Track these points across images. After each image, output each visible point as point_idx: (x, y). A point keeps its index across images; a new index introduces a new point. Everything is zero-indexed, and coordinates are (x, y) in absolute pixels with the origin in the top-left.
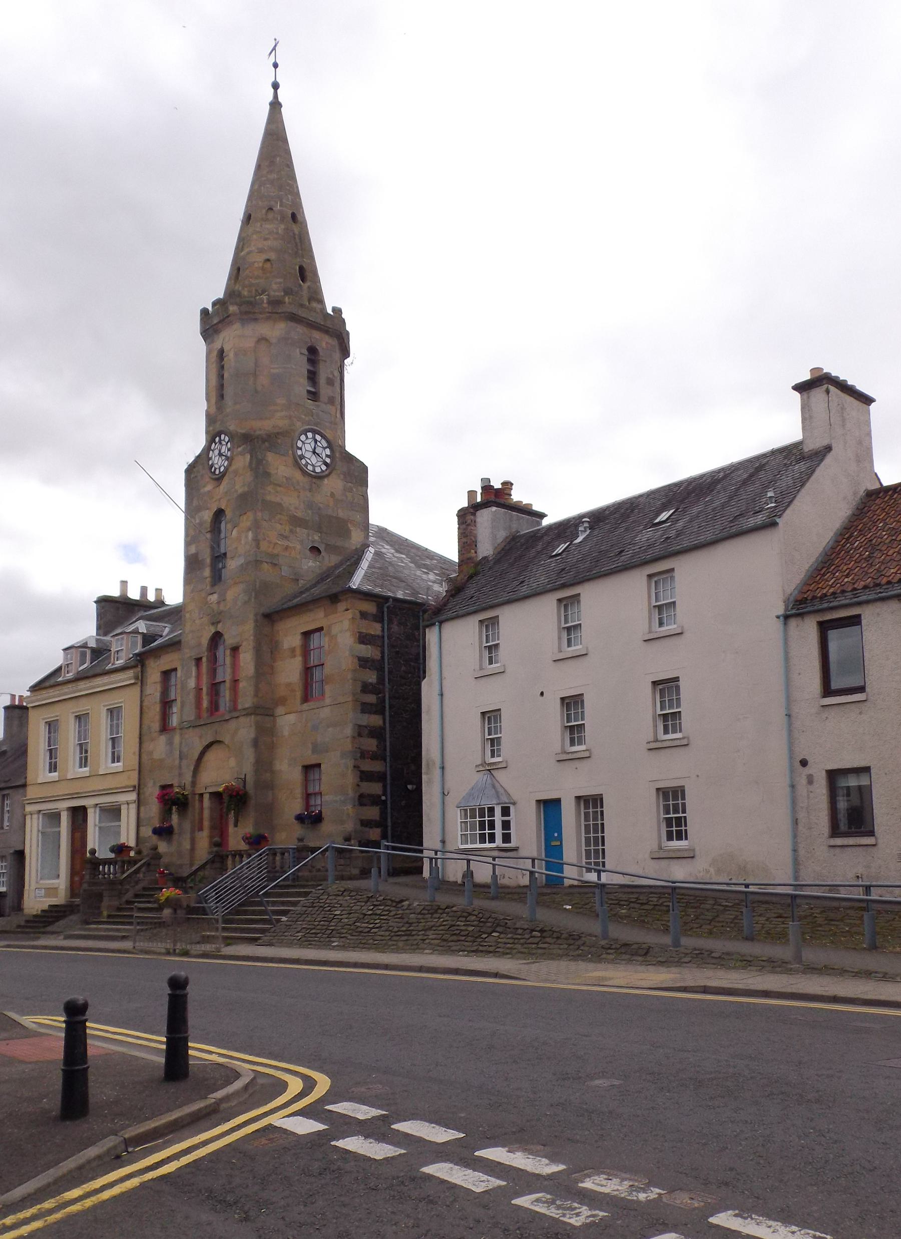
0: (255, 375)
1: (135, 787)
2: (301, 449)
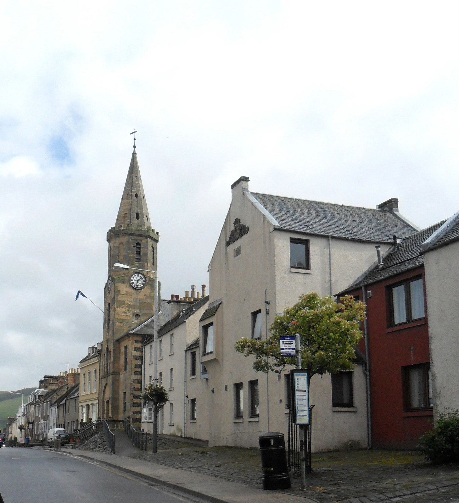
0: (119, 256)
1: (97, 398)
2: (133, 280)
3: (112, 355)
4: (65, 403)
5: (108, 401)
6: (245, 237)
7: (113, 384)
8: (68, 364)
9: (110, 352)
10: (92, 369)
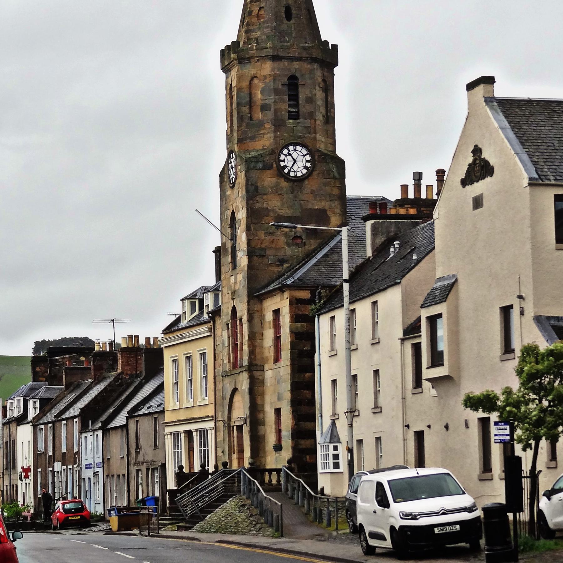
1: (212, 417)
3: (245, 326)
4: (125, 427)
5: (240, 428)
6: (488, 179)
7: (252, 391)
8: (113, 320)
9: (241, 320)
10: (195, 350)
